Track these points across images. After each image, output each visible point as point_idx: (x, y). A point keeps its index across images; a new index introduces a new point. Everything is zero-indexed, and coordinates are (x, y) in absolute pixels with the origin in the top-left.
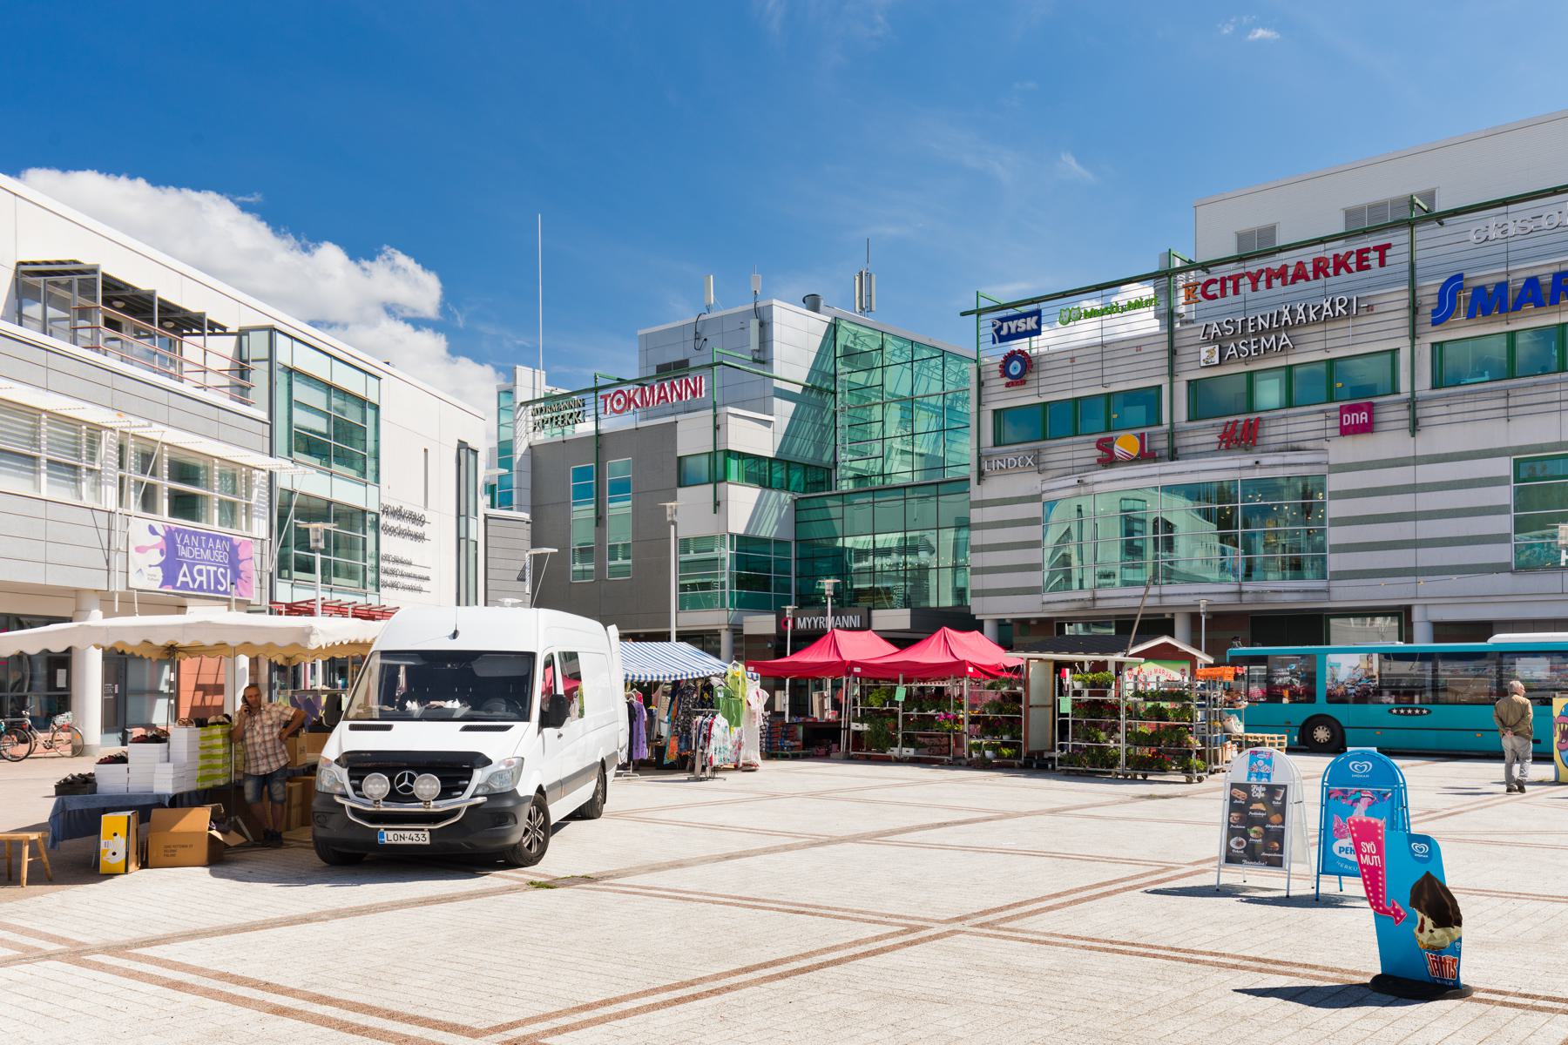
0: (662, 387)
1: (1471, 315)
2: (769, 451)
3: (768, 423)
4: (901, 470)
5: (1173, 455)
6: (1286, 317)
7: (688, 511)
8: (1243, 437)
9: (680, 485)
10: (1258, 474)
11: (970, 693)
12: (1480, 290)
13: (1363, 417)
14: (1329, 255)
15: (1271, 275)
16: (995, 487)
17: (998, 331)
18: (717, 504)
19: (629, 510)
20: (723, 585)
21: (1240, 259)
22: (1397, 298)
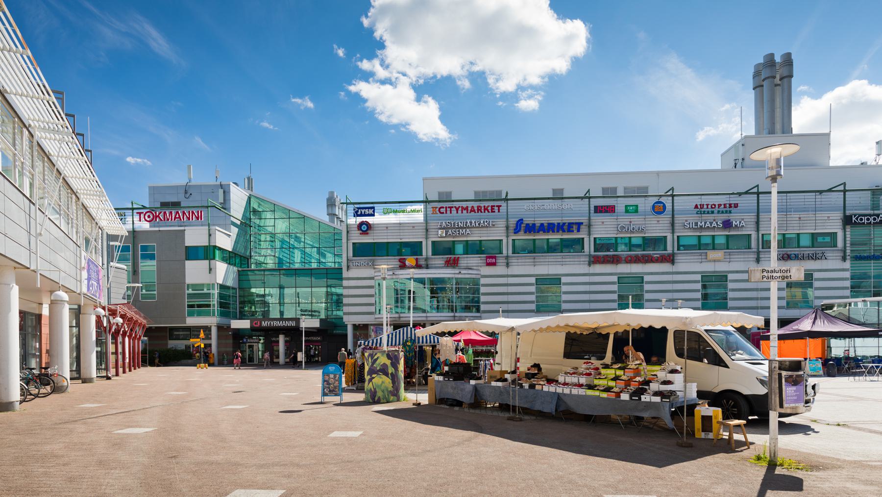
0: (177, 212)
1: (525, 232)
2: (229, 248)
3: (229, 236)
4: (270, 263)
5: (427, 267)
6: (469, 224)
7: (195, 272)
8: (453, 263)
9: (187, 259)
10: (460, 276)
11: (219, 353)
12: (527, 225)
13: (493, 260)
14: (482, 205)
15: (463, 208)
16: (354, 273)
17: (357, 212)
18: (210, 269)
19: (155, 268)
20: (214, 305)
21: (439, 201)
22: (502, 223)
